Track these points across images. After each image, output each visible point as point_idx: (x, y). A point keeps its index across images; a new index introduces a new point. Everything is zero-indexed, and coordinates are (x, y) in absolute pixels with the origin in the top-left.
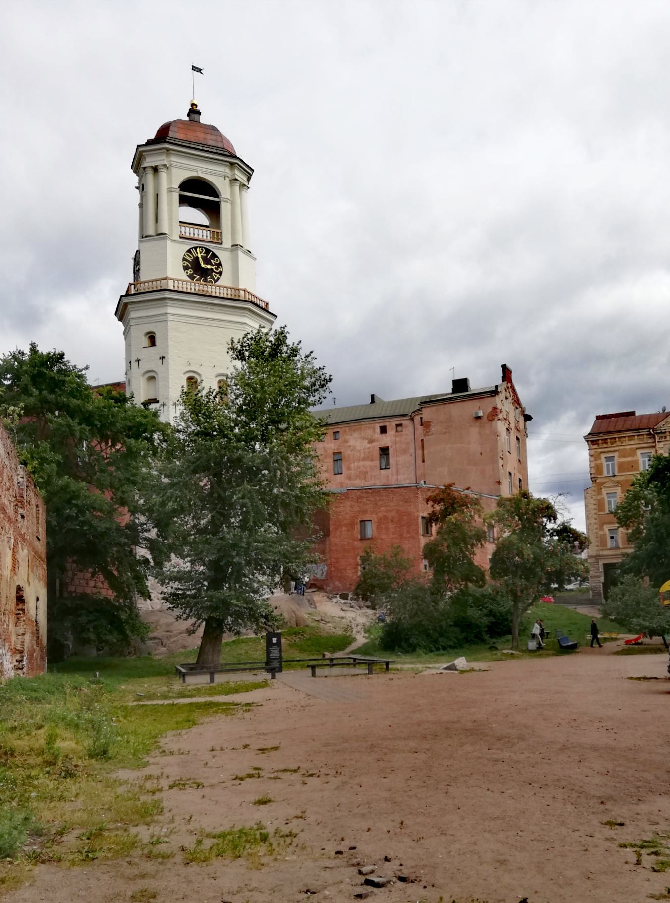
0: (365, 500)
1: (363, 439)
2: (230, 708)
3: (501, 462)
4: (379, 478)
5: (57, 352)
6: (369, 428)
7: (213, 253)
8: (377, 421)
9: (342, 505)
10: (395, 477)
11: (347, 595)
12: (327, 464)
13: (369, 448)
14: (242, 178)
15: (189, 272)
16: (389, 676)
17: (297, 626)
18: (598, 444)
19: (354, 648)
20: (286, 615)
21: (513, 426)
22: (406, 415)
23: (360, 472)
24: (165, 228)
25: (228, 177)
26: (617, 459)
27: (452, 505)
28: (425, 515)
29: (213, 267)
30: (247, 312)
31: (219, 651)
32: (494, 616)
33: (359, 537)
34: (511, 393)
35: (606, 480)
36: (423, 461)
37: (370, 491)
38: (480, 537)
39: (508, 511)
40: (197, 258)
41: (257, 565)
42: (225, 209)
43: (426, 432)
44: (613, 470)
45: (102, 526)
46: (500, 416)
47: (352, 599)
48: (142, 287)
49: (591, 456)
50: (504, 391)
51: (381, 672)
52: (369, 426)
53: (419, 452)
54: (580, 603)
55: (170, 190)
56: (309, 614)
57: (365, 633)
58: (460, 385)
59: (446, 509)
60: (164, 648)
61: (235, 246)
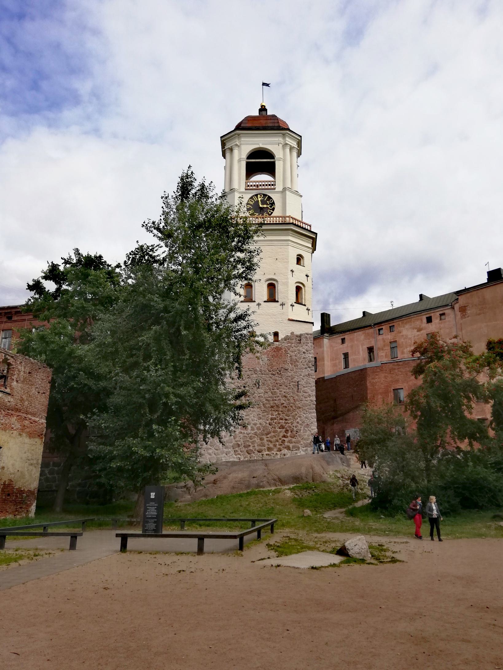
0: (396, 371)
1: (413, 329)
8: (423, 314)
9: (377, 377)
13: (418, 335)
17: (313, 481)
22: (447, 305)
25: (281, 143)
30: (290, 232)
37: (401, 363)
40: (258, 201)
43: (463, 315)
52: (417, 318)
55: (240, 161)
60: (189, 497)
61: (285, 189)
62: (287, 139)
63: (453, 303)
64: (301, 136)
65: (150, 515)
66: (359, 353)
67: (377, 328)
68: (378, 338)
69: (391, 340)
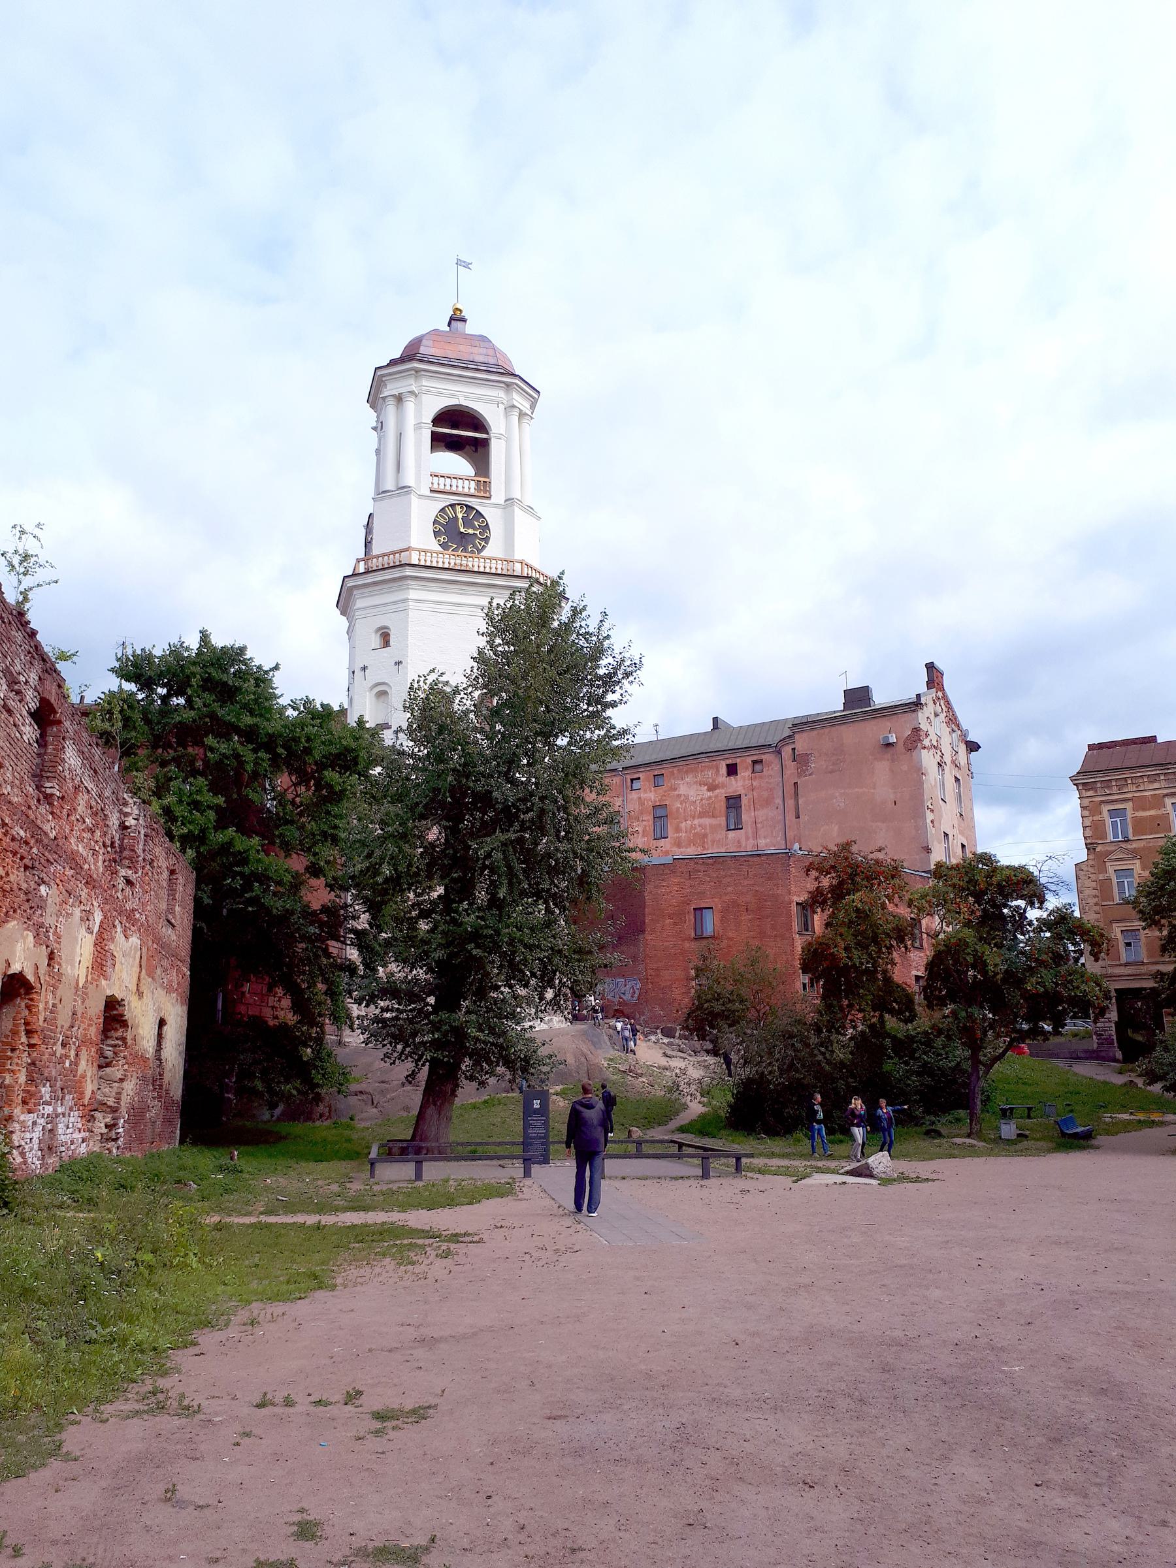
2: (416, 1245)
3: (929, 816)
4: (728, 843)
5: (237, 646)
6: (709, 768)
7: (477, 511)
10: (751, 841)
11: (674, 1030)
12: (644, 823)
13: (710, 798)
14: (523, 404)
15: (442, 540)
16: (740, 1183)
18: (1095, 789)
19: (683, 1123)
20: (570, 1060)
21: (947, 759)
23: (695, 834)
24: (409, 479)
26: (1129, 812)
27: (852, 876)
28: (803, 898)
29: (478, 532)
31: (449, 1119)
32: (931, 1074)
33: (693, 935)
34: (944, 707)
35: (1114, 849)
36: (798, 817)
38: (904, 933)
39: (954, 886)
40: (456, 518)
41: (515, 973)
42: (497, 450)
44: (1124, 830)
45: (279, 906)
46: (926, 742)
47: (680, 1037)
48: (374, 564)
49: (1083, 808)
50: (931, 703)
51: (727, 1175)
53: (790, 803)
54: (1075, 1056)
55: (419, 426)
56: (610, 1060)
57: (702, 1096)
58: (857, 698)
59: (841, 883)
60: (375, 1110)
61: (509, 500)
62: (515, 395)
63: (780, 745)
64: (539, 392)
65: (535, 1133)
67: (629, 777)
68: (630, 797)
69: (655, 801)
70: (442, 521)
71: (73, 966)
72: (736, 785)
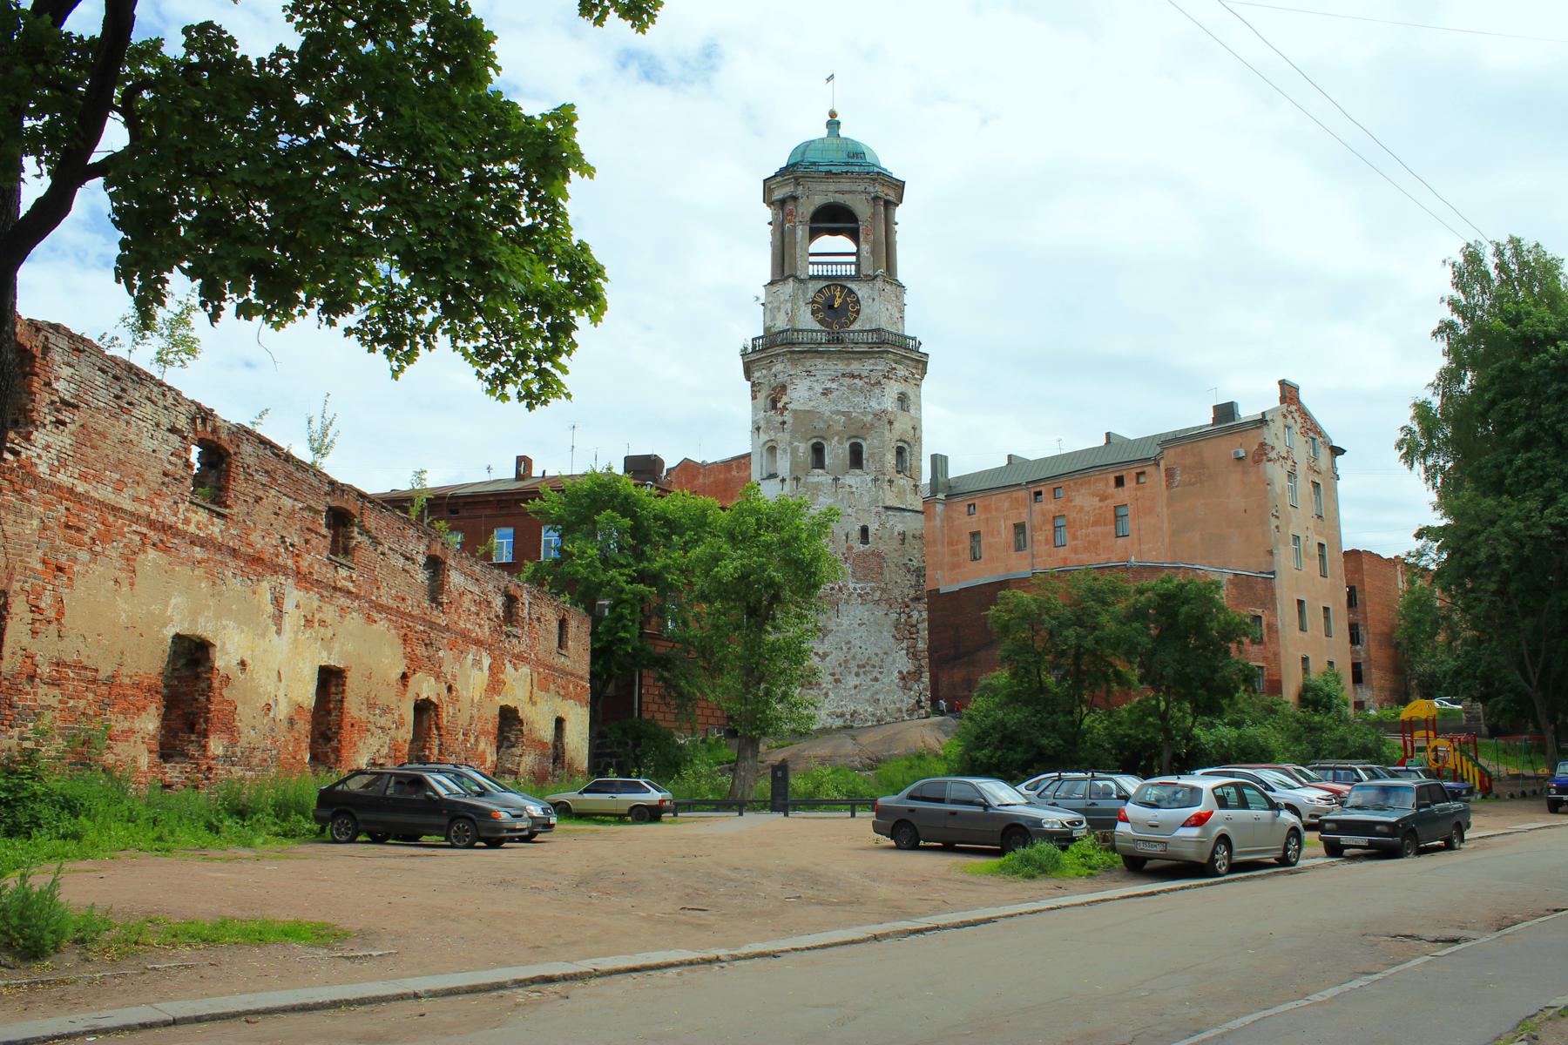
3: (1274, 522)
13: (1101, 508)
23: (1089, 542)
58: (1225, 412)
66: (999, 533)
70: (819, 300)
71: (468, 690)
72: (1123, 495)
